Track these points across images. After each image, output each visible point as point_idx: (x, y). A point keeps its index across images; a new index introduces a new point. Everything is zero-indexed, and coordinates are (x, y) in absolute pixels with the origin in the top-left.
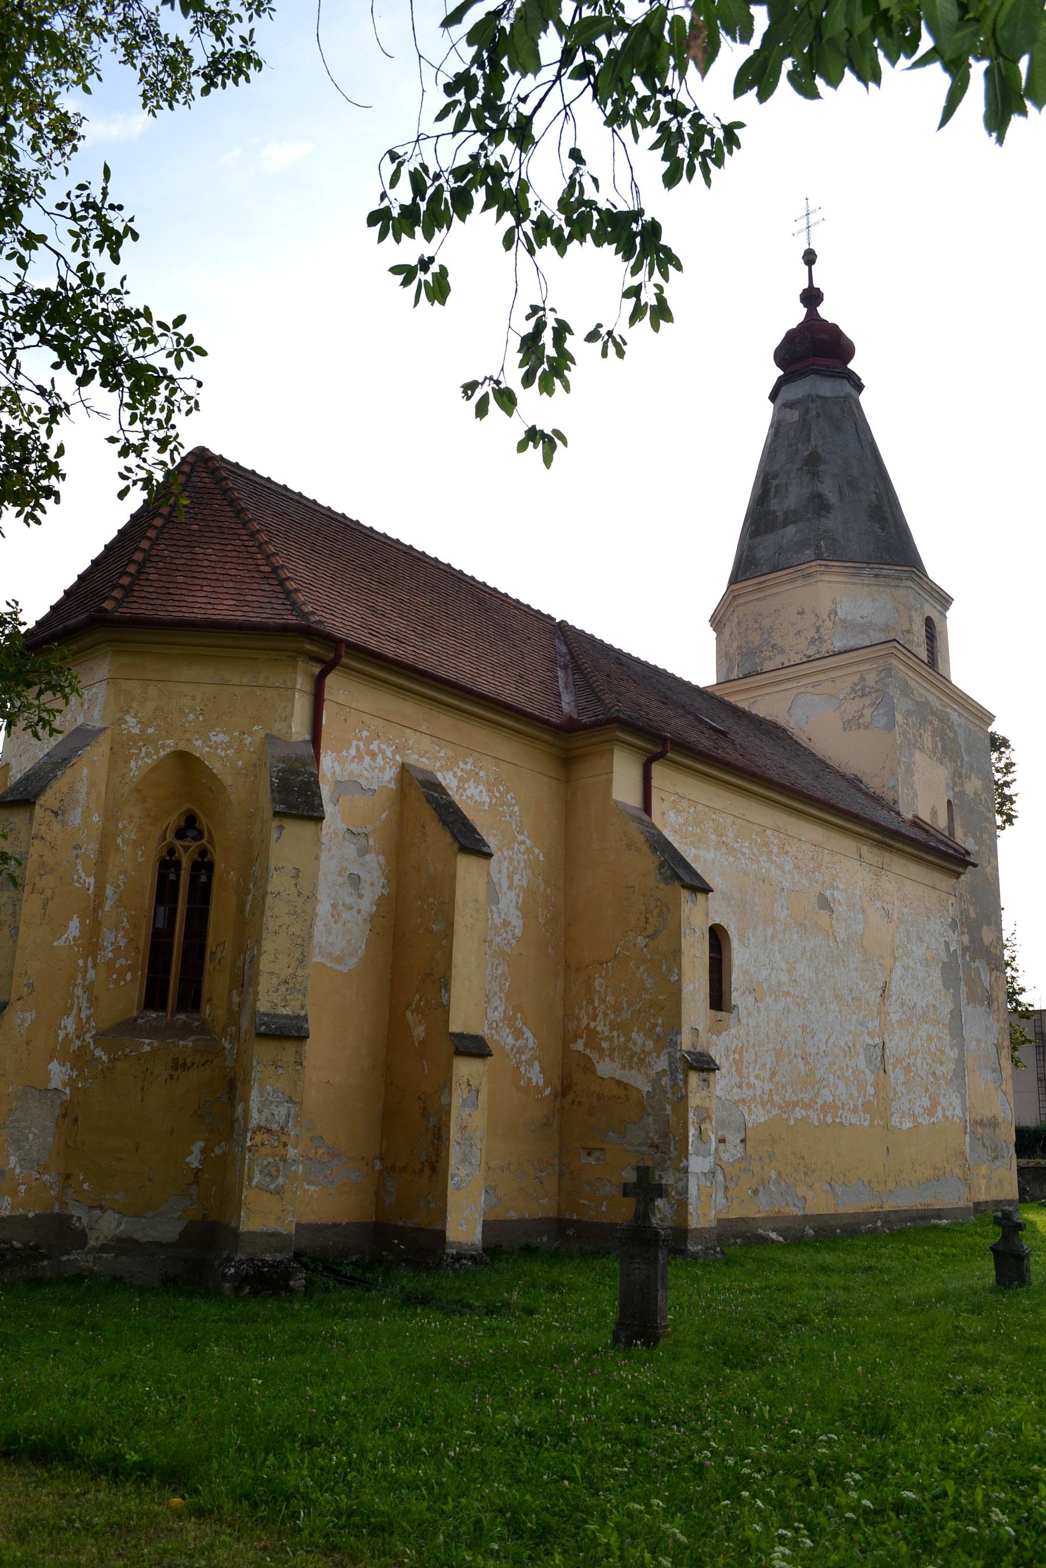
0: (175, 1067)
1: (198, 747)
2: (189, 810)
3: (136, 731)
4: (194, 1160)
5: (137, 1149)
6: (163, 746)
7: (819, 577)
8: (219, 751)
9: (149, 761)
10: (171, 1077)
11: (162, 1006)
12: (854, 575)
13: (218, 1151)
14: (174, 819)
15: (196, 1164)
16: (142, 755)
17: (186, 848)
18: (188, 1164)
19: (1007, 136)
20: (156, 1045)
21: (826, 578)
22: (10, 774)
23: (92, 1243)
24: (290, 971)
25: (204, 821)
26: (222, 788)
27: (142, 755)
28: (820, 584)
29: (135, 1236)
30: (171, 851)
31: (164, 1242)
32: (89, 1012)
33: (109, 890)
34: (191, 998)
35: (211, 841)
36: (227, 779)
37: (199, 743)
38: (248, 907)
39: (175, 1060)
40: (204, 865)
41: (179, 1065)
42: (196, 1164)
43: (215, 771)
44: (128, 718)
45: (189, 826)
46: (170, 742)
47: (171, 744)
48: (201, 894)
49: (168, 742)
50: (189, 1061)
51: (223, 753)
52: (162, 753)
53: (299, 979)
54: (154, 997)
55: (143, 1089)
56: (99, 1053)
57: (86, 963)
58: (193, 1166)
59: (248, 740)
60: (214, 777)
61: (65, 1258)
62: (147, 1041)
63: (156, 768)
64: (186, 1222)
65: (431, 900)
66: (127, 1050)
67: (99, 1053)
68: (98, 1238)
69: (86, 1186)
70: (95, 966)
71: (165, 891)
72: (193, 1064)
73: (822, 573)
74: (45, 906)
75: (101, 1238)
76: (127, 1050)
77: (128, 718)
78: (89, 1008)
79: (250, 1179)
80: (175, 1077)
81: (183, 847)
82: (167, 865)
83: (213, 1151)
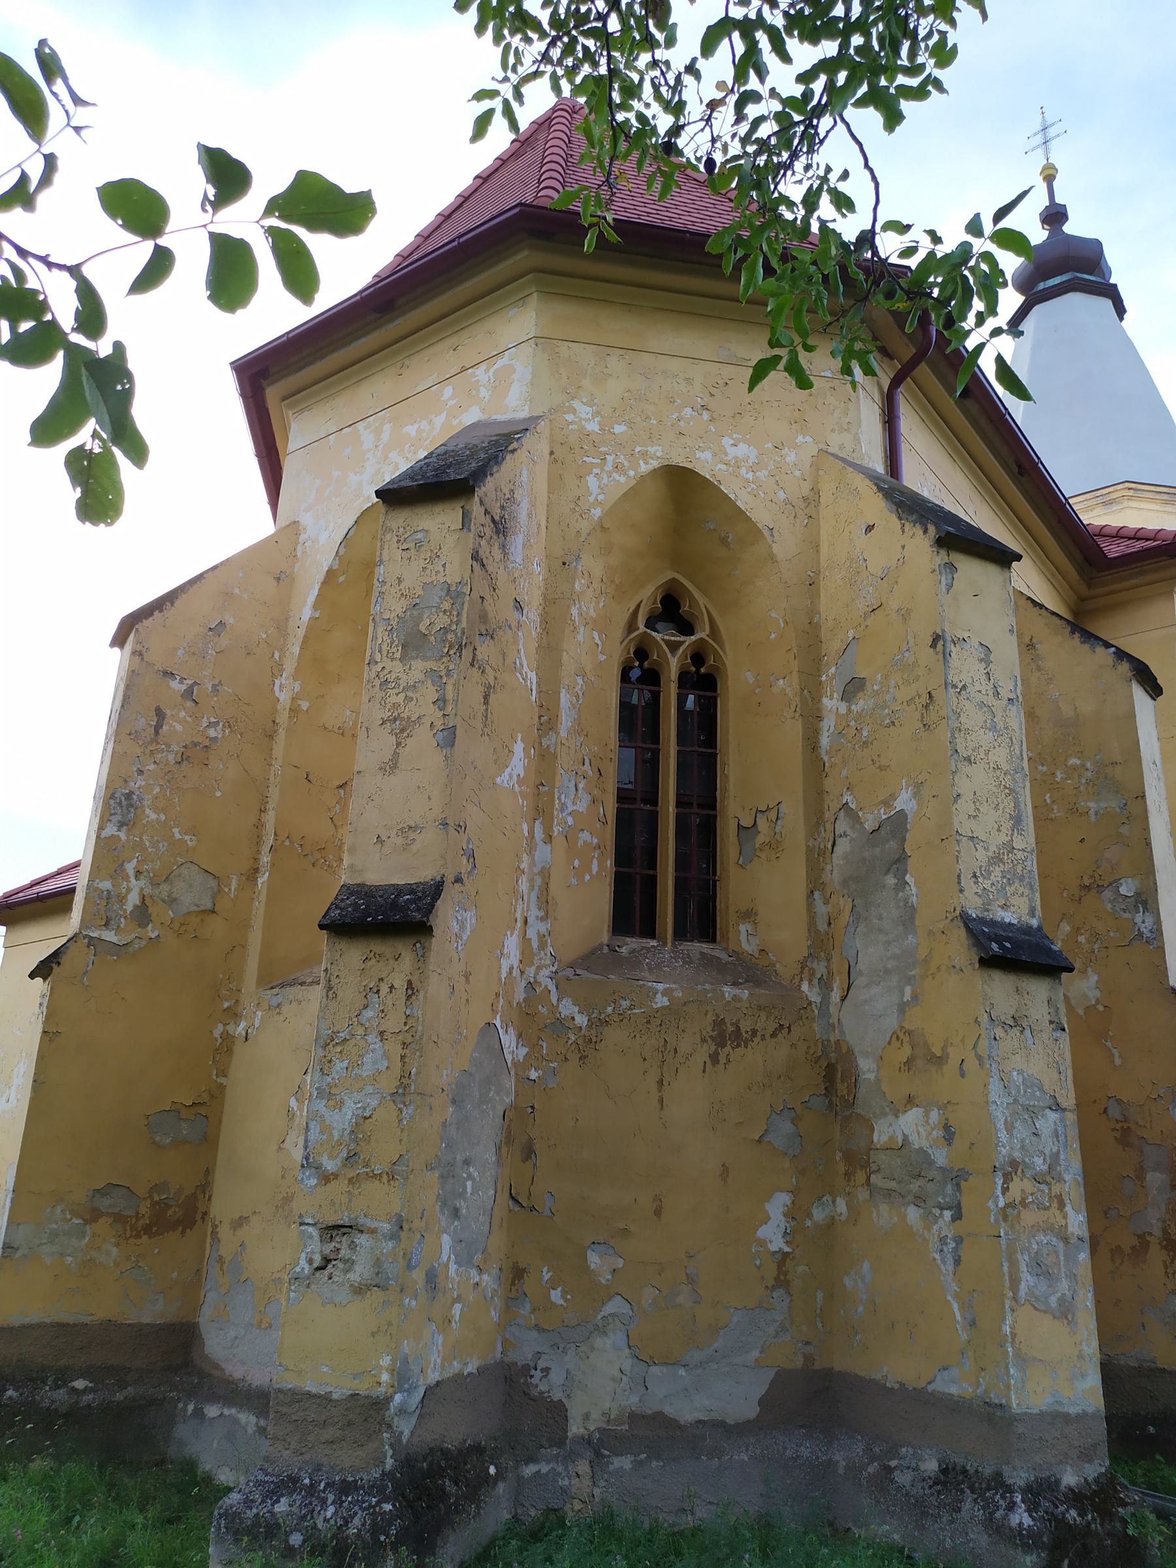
0: (720, 1040)
1: (705, 463)
2: (674, 580)
3: (593, 427)
4: (772, 1234)
5: (658, 1213)
6: (644, 455)
7: (1126, 504)
8: (743, 471)
9: (622, 479)
10: (714, 1057)
11: (649, 930)
12: (1166, 502)
13: (819, 1215)
14: (647, 595)
15: (777, 1243)
16: (609, 467)
17: (674, 646)
18: (763, 1243)
19: (26, 881)
20: (679, 994)
21: (1134, 504)
22: (302, 538)
23: (575, 1429)
24: (1003, 838)
25: (700, 601)
26: (754, 532)
27: (609, 467)
28: (1127, 510)
29: (669, 1410)
30: (641, 653)
31: (730, 1422)
32: (543, 927)
33: (565, 699)
34: (701, 918)
35: (714, 632)
36: (761, 515)
37: (706, 456)
38: (255, 940)
39: (719, 1023)
40: (703, 680)
41: (726, 1037)
42: (777, 1243)
43: (739, 503)
44: (576, 404)
45: (672, 610)
46: (656, 450)
47: (657, 455)
48: (703, 729)
49: (651, 450)
50: (746, 1025)
51: (750, 476)
52: (644, 468)
53: (1020, 855)
54: (632, 911)
55: (660, 1083)
56: (567, 1008)
57: (531, 831)
58: (773, 1248)
59: (791, 457)
60: (740, 515)
61: (529, 1470)
62: (660, 987)
63: (630, 494)
64: (771, 1374)
65: (1074, 761)
66: (625, 1004)
67: (567, 1008)
68: (587, 1417)
69: (556, 1296)
70: (549, 839)
71: (637, 723)
72: (754, 1033)
73: (1131, 498)
74: (486, 697)
75: (593, 1416)
76: (625, 1004)
77: (576, 404)
78: (542, 919)
79: (1015, 1283)
80: (722, 1060)
81: (667, 643)
82: (640, 672)
83: (809, 1215)
